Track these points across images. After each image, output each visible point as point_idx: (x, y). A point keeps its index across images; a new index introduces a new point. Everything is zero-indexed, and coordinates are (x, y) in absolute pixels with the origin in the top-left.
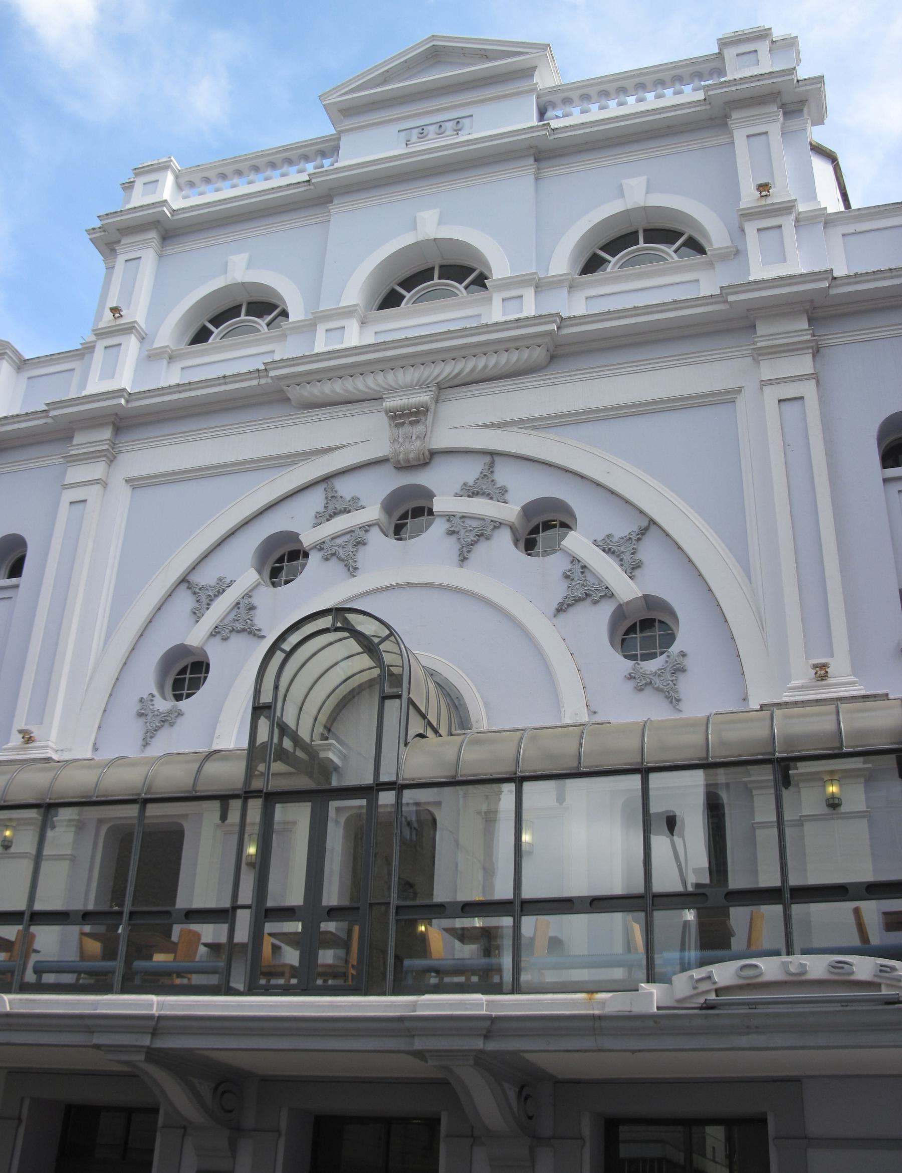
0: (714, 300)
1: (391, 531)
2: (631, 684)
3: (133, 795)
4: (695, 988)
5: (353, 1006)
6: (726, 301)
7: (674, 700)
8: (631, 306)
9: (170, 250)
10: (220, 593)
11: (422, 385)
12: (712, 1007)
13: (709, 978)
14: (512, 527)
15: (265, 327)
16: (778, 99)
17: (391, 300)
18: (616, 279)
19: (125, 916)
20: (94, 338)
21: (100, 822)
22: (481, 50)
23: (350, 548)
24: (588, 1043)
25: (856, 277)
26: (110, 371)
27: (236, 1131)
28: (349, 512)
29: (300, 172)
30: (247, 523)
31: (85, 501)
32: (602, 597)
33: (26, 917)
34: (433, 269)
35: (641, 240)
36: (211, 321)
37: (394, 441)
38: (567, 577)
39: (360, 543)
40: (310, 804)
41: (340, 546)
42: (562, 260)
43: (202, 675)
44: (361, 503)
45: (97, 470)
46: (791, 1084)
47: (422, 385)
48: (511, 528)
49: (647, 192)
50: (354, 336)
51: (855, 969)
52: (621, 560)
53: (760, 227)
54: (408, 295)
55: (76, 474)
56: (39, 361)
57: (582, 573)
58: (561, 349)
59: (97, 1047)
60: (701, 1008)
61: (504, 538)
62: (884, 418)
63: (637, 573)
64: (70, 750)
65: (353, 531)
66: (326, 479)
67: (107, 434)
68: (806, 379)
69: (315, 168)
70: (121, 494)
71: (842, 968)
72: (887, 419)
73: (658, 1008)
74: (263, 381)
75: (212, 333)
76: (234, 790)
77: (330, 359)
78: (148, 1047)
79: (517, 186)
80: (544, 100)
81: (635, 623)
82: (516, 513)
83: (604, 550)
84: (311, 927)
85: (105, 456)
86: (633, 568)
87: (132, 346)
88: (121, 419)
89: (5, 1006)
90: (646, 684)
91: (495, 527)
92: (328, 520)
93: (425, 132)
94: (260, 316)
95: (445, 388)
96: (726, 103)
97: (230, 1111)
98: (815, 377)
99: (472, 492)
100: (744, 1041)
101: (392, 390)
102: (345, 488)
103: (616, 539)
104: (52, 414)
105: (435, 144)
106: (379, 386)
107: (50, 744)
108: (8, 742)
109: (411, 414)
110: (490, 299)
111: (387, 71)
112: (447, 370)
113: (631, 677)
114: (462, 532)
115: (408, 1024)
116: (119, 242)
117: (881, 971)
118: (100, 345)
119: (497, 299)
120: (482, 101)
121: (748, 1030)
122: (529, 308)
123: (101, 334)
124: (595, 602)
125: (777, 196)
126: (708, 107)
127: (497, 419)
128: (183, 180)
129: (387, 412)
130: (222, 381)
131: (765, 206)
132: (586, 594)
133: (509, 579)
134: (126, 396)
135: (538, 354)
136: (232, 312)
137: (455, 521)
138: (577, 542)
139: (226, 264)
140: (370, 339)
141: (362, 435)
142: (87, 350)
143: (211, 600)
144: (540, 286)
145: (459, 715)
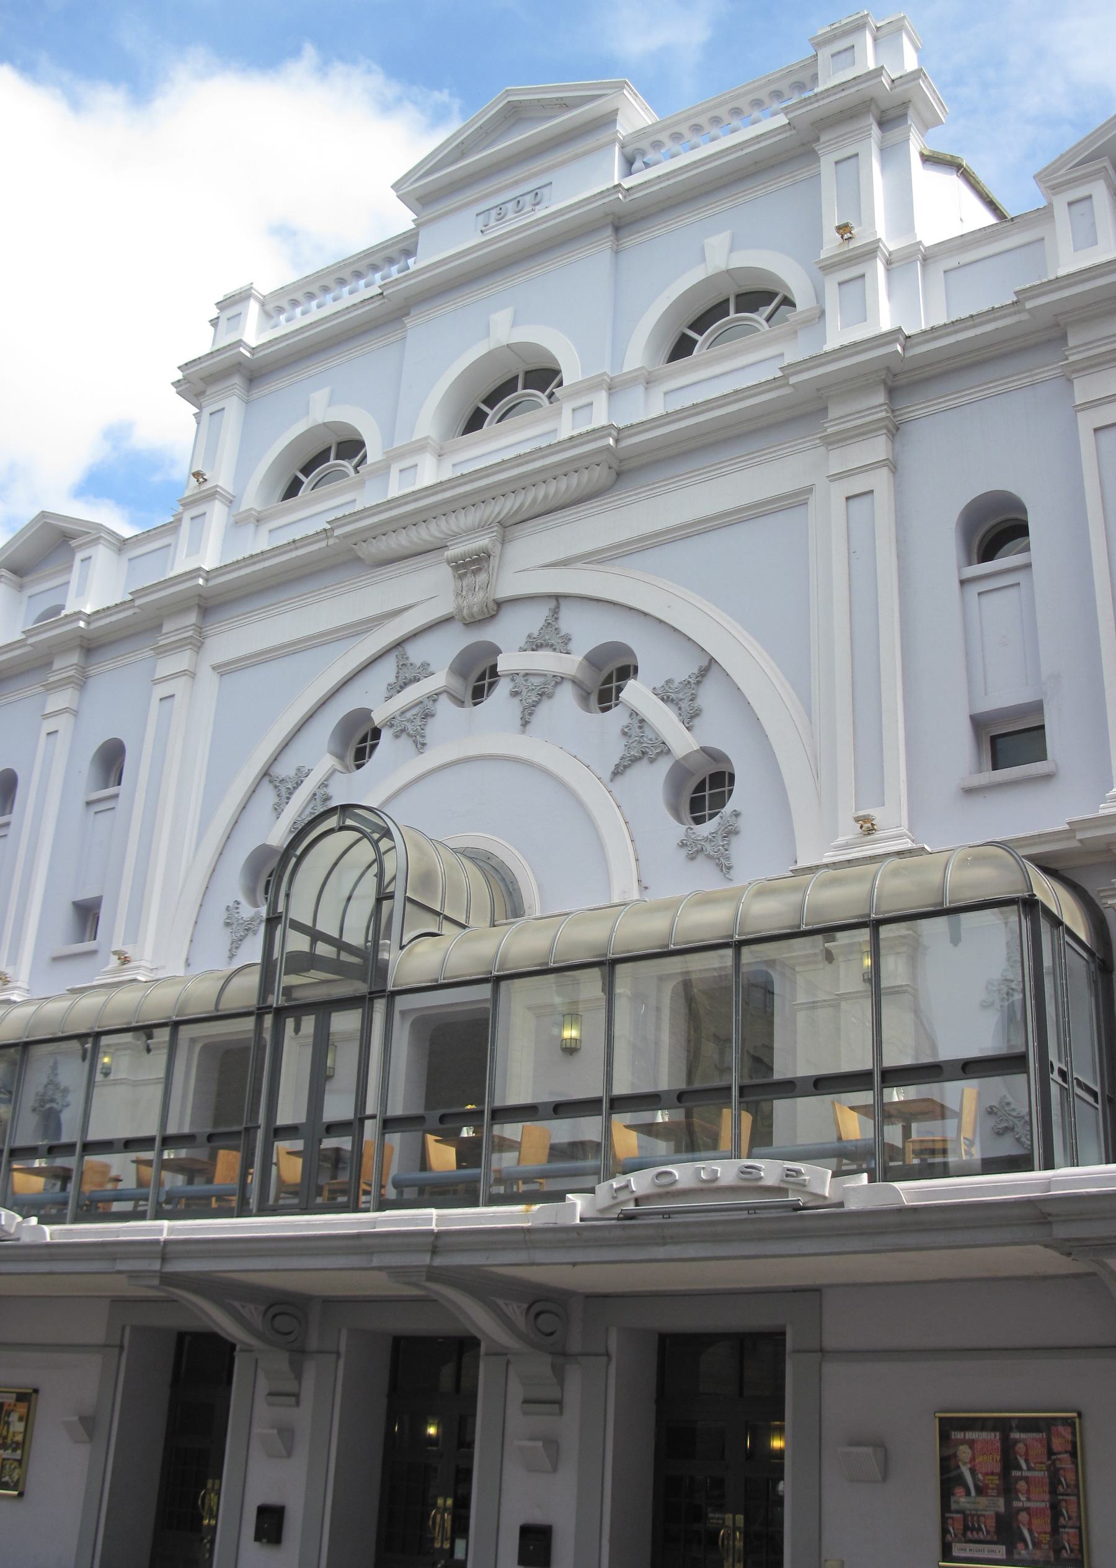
0: (777, 384)
1: (468, 698)
2: (683, 852)
3: (722, 938)
4: (614, 1198)
5: (326, 1225)
6: (788, 384)
7: (725, 868)
8: (690, 404)
9: (256, 393)
10: (299, 784)
11: (483, 526)
12: (798, 1208)
13: (627, 1186)
14: (574, 682)
15: (764, 323)
16: (873, 107)
17: (475, 422)
18: (708, 363)
19: (735, 1092)
20: (181, 509)
21: (661, 979)
22: (557, 99)
23: (418, 722)
24: (522, 1256)
25: (933, 332)
26: (196, 546)
27: (561, 1357)
28: (419, 680)
29: (367, 285)
30: (324, 703)
31: (872, 491)
32: (658, 754)
33: (877, 1078)
34: (727, 300)
35: (520, 385)
36: (691, 327)
37: (458, 595)
38: (625, 734)
39: (427, 715)
40: (313, 1017)
41: (409, 720)
42: (638, 351)
43: (727, 789)
44: (431, 669)
45: (182, 661)
46: (811, 1295)
47: (483, 526)
48: (573, 682)
49: (731, 250)
50: (428, 473)
51: (762, 1174)
52: (680, 709)
53: (1070, 199)
54: (700, 339)
55: (1085, 389)
56: (137, 540)
57: (640, 727)
58: (624, 466)
59: (119, 1272)
60: (618, 1219)
61: (566, 696)
62: (101, 743)
63: (696, 722)
64: (164, 967)
65: (421, 702)
66: (398, 644)
67: (192, 618)
68: (877, 468)
69: (399, 272)
70: (208, 680)
71: (750, 1173)
72: (969, 504)
73: (582, 1220)
74: (331, 542)
75: (696, 341)
76: (248, 1007)
77: (390, 509)
78: (160, 1271)
79: (593, 263)
80: (629, 150)
81: (704, 780)
82: (576, 665)
83: (663, 699)
84: (313, 1143)
85: (190, 643)
86: (690, 718)
87: (217, 512)
88: (206, 599)
89: (45, 1238)
90: (697, 852)
91: (557, 684)
92: (399, 692)
93: (503, 212)
94: (754, 309)
95: (508, 527)
96: (813, 124)
97: (551, 1334)
98: (893, 465)
99: (535, 645)
100: (660, 1252)
101: (455, 535)
102: (416, 653)
103: (676, 684)
104: (138, 603)
105: (516, 225)
106: (442, 532)
107: (143, 963)
108: (107, 964)
109: (473, 562)
110: (559, 413)
111: (462, 143)
112: (507, 506)
113: (683, 845)
114: (409, 726)
115: (365, 1241)
116: (818, 139)
117: (787, 1176)
118: (187, 516)
119: (567, 409)
120: (563, 163)
121: (664, 1241)
122: (600, 417)
123: (188, 504)
124: (652, 761)
125: (861, 239)
126: (794, 132)
127: (562, 556)
128: (270, 307)
129: (449, 562)
130: (293, 546)
131: (845, 252)
132: (643, 753)
133: (571, 741)
134: (204, 575)
135: (600, 475)
136: (718, 311)
137: (520, 680)
138: (634, 692)
139: (703, 249)
140: (447, 474)
141: (425, 591)
142: (173, 527)
143: (291, 793)
144: (613, 388)
145: (509, 902)
